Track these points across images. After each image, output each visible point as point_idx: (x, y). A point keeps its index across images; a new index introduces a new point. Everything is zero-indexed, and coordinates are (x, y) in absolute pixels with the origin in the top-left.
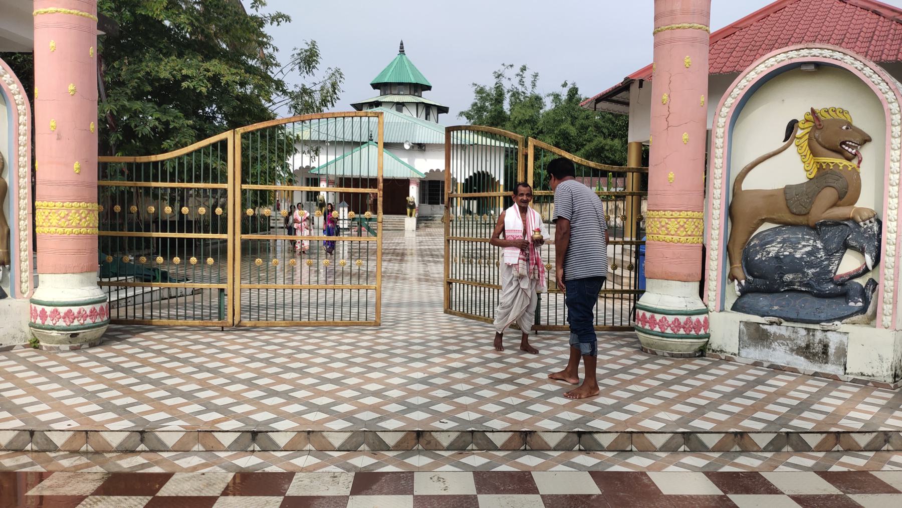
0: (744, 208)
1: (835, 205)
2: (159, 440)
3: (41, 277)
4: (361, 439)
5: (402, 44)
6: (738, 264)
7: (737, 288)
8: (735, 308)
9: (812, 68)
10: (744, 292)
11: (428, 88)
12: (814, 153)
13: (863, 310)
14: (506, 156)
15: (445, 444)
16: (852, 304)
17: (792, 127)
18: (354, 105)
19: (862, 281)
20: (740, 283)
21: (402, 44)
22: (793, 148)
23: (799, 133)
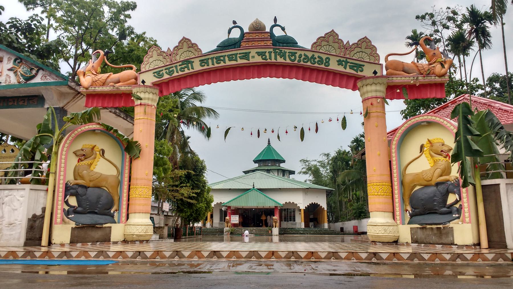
0: (407, 179)
1: (441, 176)
2: (182, 254)
3: (130, 215)
4: (253, 254)
5: (269, 140)
6: (407, 203)
7: (408, 214)
8: (409, 223)
9: (425, 123)
10: (412, 216)
11: (284, 161)
12: (432, 156)
13: (459, 218)
14: (327, 196)
15: (283, 256)
16: (454, 216)
17: (422, 147)
18: (244, 172)
19: (457, 206)
20: (409, 212)
21: (269, 140)
22: (423, 155)
23: (425, 149)
